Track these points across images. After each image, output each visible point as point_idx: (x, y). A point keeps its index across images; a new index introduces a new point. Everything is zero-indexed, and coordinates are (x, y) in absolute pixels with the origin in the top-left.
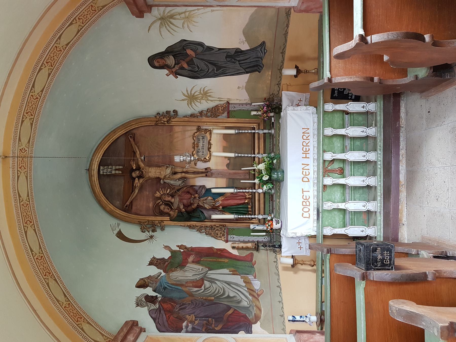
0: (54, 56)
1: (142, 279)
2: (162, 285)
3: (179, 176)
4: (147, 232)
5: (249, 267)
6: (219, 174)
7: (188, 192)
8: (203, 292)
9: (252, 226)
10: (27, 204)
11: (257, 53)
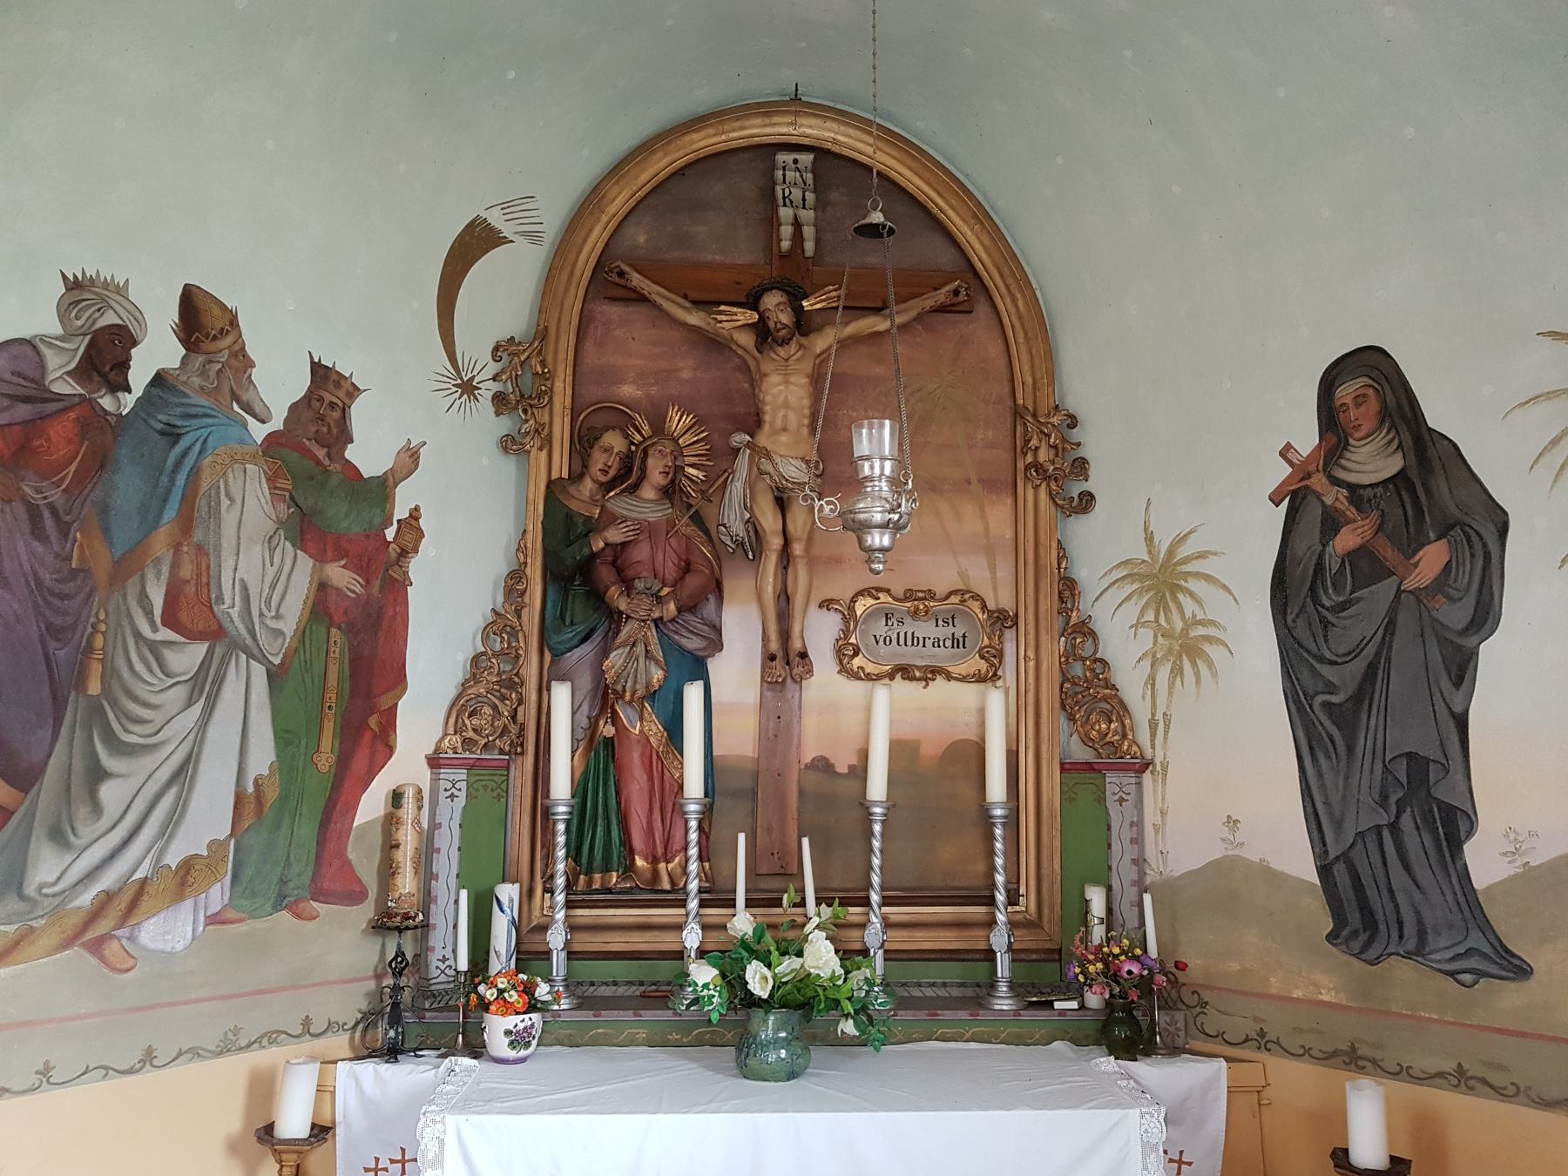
1: (233, 321)
2: (195, 423)
3: (769, 520)
4: (493, 368)
5: (283, 882)
7: (687, 568)
8: (138, 635)
9: (508, 893)
11: (1451, 927)
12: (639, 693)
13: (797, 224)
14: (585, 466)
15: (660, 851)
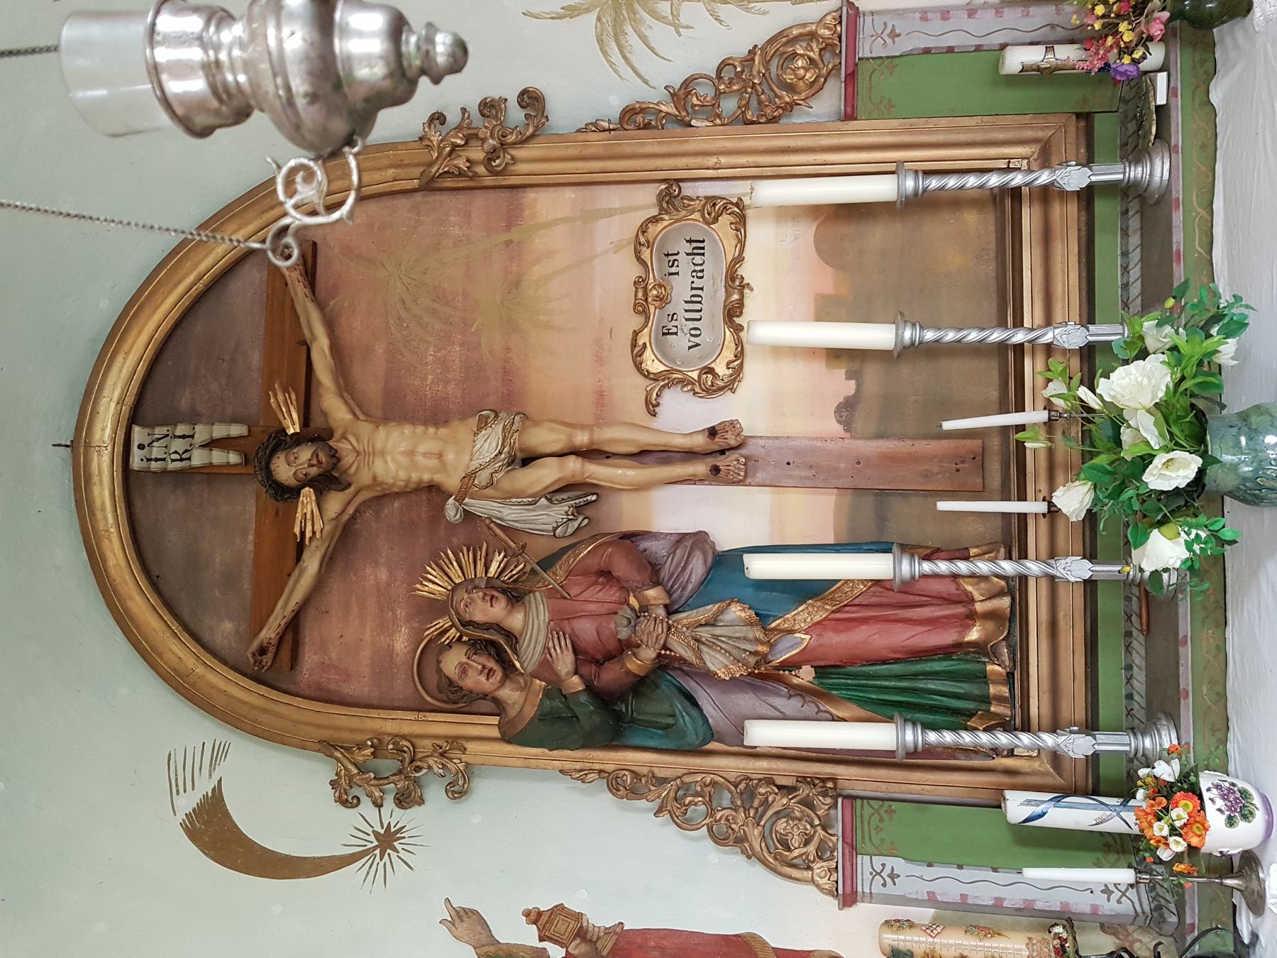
3: (546, 474)
4: (366, 807)
6: (801, 467)
7: (605, 574)
9: (1017, 806)
12: (759, 634)
13: (211, 444)
14: (485, 696)
15: (960, 610)
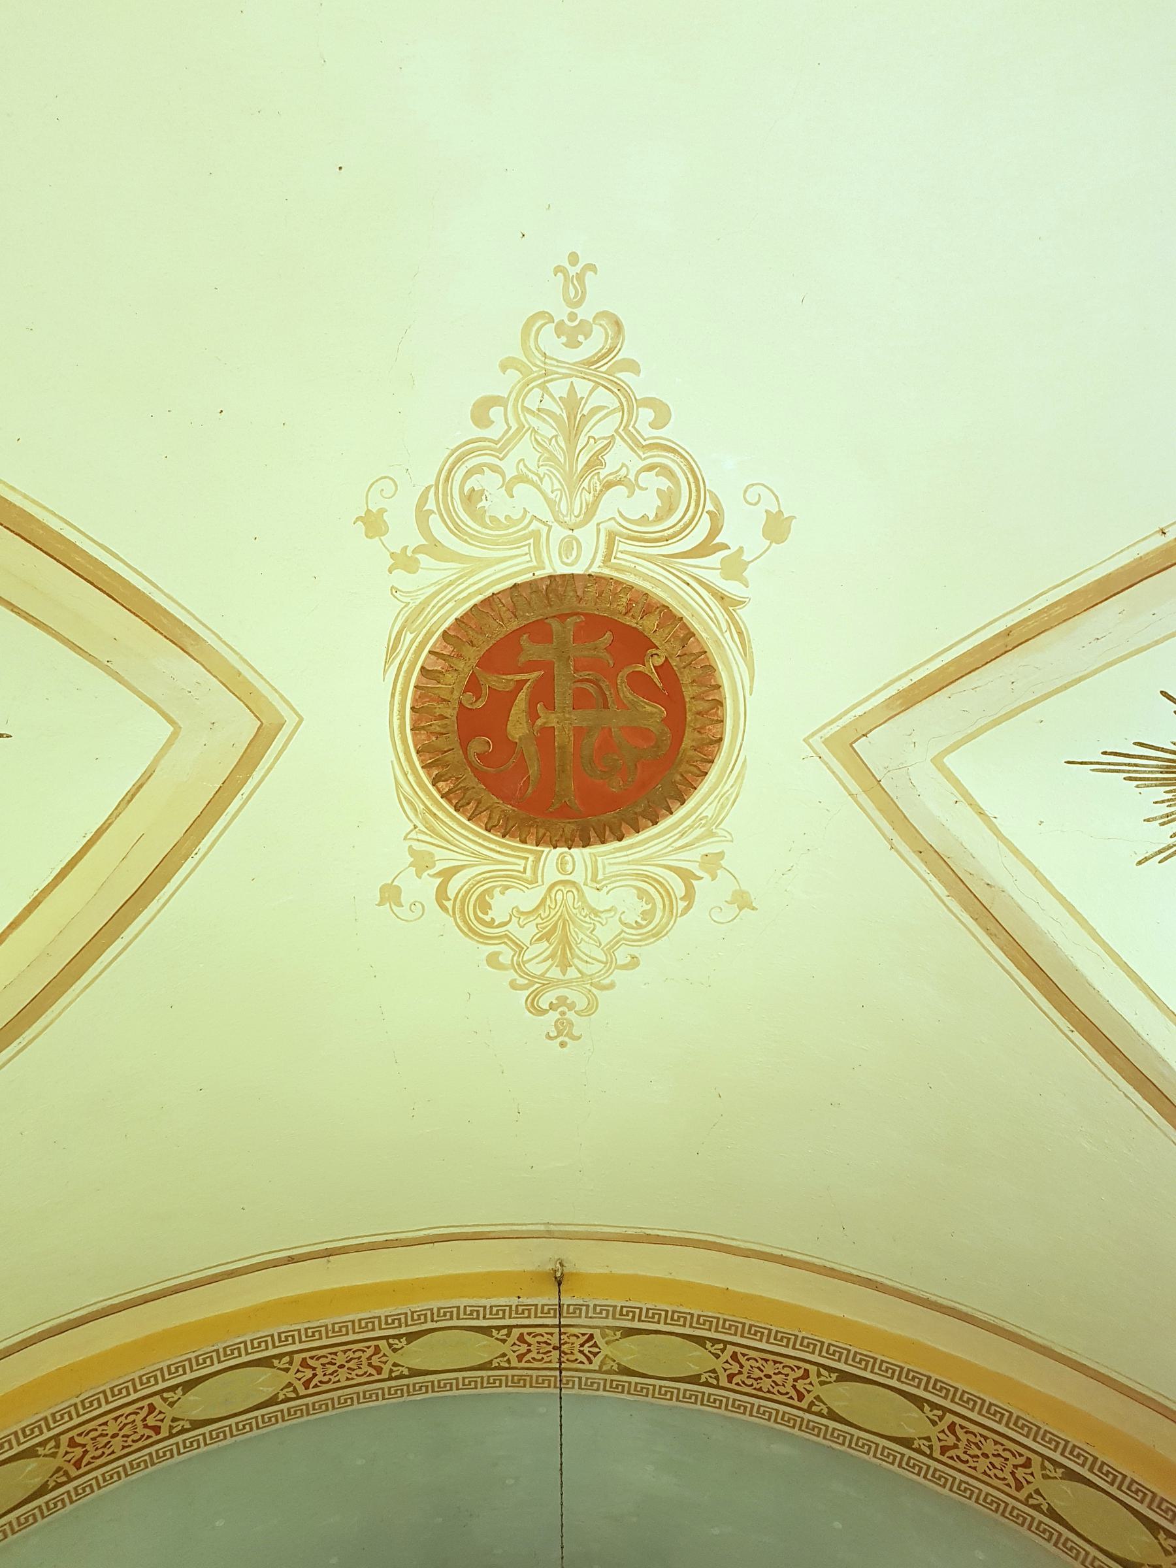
0: (986, 1456)
10: (379, 1370)
